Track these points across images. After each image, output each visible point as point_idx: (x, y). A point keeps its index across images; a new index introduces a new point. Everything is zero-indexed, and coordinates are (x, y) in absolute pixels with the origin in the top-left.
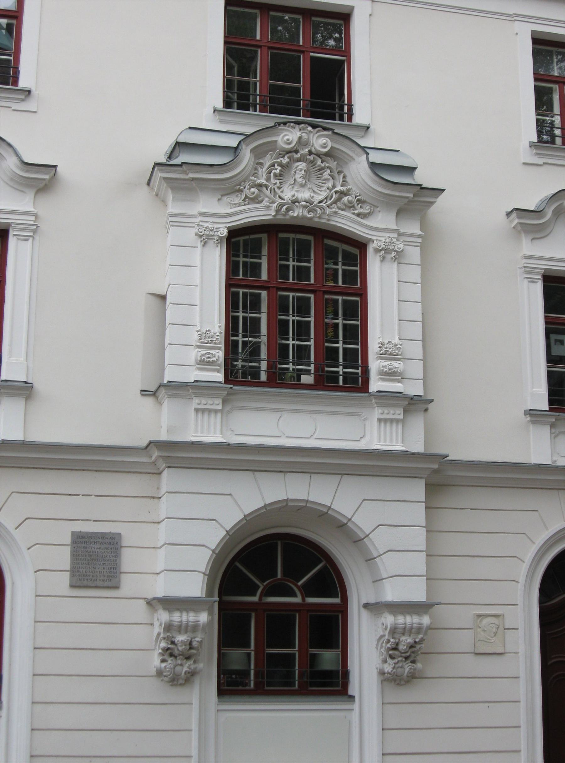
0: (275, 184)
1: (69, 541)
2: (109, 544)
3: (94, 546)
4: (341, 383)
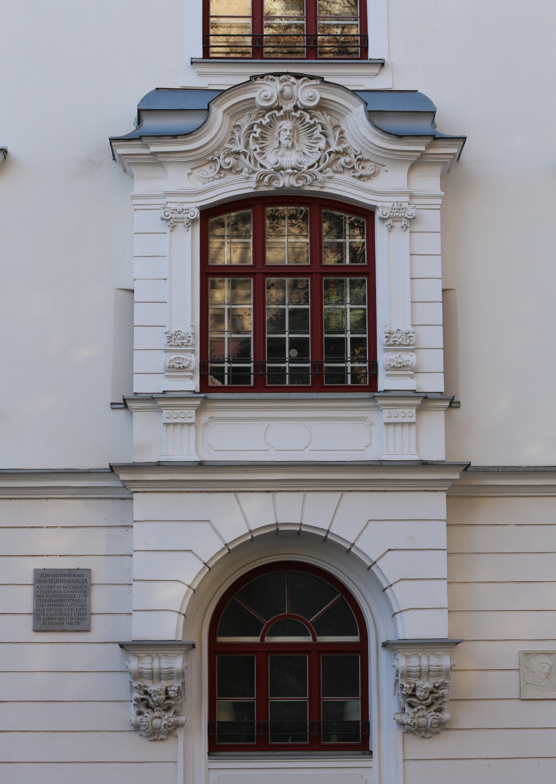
0: (255, 150)
1: (31, 581)
2: (77, 582)
3: (60, 585)
4: (349, 383)
